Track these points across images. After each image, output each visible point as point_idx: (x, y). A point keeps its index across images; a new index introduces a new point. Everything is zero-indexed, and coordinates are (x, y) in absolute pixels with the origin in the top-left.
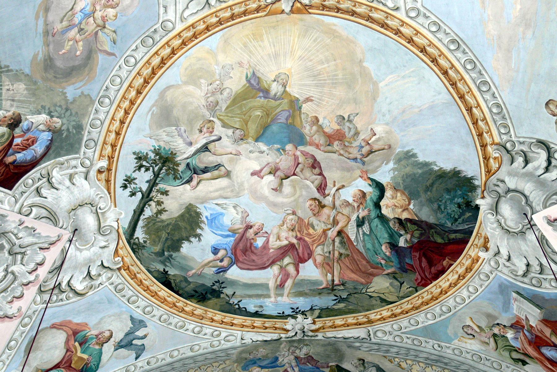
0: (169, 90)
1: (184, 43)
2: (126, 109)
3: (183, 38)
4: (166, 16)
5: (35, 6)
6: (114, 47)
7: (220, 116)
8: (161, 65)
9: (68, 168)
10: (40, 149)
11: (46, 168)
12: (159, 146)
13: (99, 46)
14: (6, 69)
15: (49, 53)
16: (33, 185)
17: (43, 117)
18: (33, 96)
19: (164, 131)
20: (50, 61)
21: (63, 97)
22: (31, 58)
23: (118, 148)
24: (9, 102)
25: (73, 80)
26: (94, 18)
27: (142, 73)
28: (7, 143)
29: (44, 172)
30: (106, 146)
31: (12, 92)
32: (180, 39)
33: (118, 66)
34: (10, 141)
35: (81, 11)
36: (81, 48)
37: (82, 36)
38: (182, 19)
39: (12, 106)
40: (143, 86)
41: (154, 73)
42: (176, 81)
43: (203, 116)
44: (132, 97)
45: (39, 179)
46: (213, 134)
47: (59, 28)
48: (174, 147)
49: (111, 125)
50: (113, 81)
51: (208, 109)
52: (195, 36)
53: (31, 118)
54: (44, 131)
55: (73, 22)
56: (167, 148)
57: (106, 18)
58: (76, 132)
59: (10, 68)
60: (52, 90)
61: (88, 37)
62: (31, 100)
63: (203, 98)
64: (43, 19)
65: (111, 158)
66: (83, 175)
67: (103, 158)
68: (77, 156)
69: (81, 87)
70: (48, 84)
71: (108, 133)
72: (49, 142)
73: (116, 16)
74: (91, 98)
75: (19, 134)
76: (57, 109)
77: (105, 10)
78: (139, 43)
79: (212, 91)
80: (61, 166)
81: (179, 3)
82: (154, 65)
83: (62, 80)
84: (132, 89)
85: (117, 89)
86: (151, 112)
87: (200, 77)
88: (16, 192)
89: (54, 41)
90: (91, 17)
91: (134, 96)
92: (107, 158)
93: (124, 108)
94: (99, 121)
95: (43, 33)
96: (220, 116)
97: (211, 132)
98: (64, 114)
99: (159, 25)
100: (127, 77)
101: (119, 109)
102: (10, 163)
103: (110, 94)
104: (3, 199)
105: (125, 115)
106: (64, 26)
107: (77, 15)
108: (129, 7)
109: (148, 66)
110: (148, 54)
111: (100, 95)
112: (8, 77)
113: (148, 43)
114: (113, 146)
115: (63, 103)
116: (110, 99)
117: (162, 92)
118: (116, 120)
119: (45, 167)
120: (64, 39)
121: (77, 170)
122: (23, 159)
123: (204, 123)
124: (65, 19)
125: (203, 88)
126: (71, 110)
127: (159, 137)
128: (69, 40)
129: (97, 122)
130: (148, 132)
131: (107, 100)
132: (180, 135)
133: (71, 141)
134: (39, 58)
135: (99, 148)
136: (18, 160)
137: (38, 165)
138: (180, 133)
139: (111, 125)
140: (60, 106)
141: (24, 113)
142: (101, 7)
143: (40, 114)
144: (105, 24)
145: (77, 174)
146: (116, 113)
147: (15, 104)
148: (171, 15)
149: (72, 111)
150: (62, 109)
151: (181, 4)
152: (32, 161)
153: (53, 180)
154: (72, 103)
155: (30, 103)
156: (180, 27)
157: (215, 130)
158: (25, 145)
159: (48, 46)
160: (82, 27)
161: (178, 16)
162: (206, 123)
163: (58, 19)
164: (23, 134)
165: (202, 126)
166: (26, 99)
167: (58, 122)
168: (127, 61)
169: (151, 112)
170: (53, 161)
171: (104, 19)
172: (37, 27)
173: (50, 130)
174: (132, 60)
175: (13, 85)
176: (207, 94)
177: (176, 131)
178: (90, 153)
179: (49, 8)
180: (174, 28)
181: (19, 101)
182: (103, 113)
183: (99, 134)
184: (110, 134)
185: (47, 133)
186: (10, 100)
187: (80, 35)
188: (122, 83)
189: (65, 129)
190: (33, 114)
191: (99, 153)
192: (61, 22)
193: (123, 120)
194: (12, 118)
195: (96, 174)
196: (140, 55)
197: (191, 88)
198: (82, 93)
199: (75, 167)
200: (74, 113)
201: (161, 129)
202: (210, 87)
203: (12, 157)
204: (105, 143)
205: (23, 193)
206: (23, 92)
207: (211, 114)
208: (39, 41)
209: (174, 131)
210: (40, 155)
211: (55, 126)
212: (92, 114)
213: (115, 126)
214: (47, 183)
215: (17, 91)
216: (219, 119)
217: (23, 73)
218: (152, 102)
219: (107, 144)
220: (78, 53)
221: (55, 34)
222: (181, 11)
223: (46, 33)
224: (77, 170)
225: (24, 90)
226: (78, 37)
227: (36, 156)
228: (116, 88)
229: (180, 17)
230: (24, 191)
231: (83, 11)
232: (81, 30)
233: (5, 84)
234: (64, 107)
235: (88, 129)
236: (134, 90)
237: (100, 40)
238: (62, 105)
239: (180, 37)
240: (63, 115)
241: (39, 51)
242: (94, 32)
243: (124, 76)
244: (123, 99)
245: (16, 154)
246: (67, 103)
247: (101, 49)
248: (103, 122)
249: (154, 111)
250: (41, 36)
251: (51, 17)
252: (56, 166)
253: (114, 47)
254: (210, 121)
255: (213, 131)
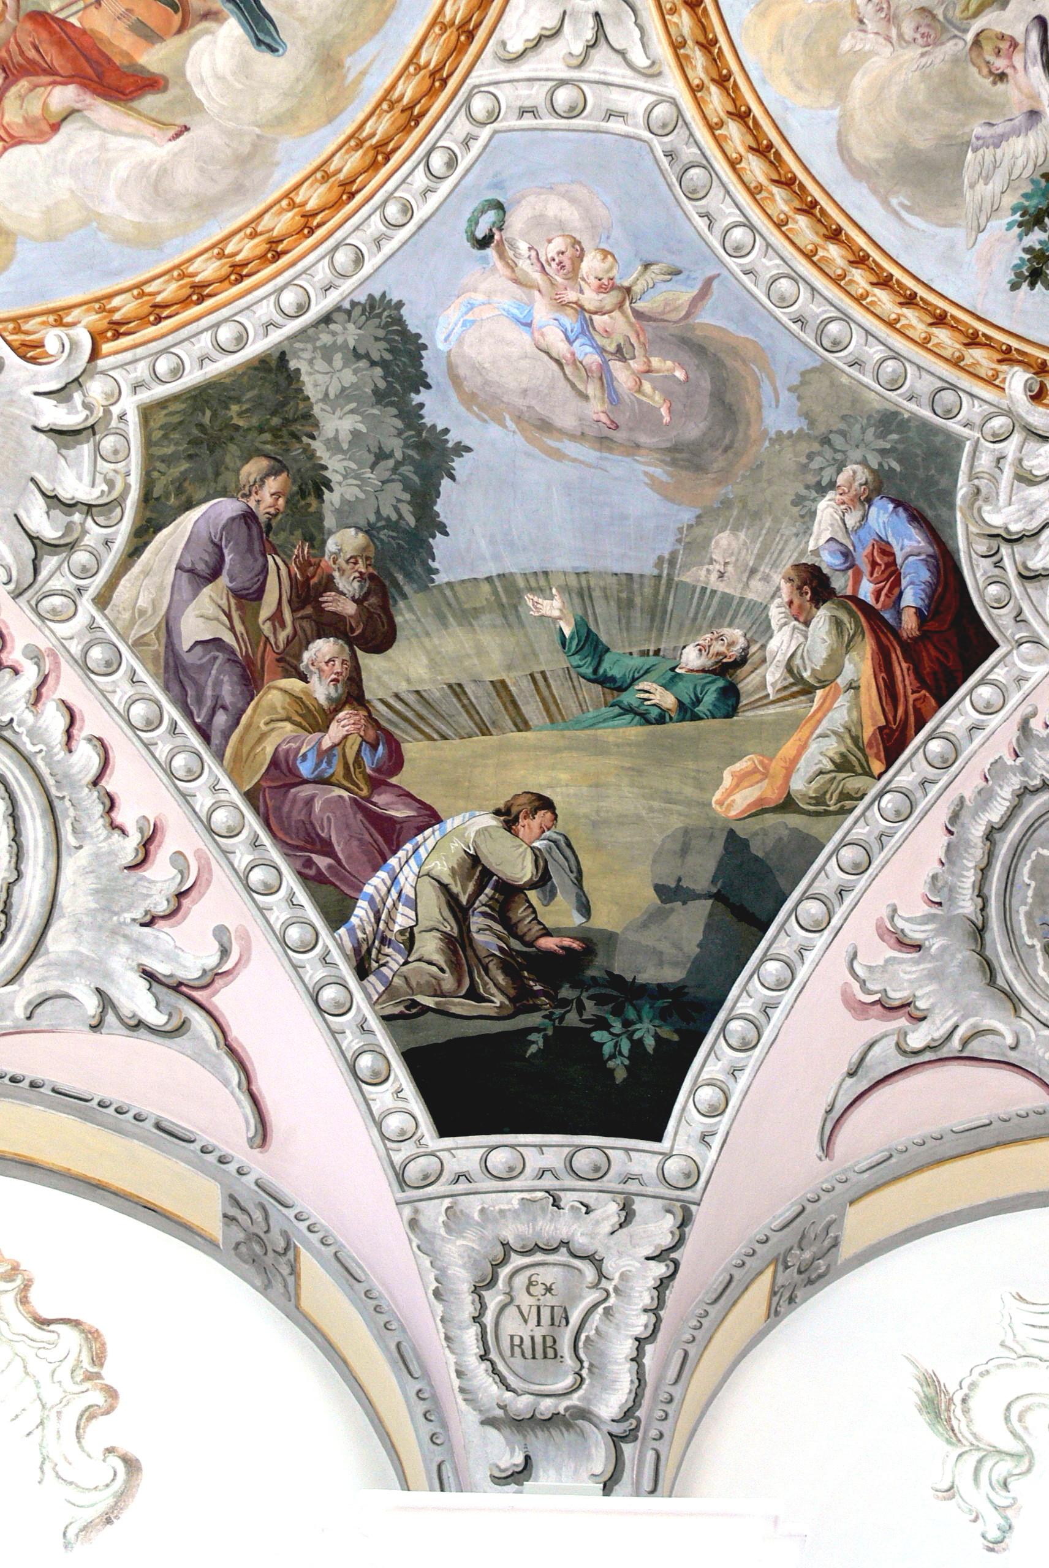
0: (849, 150)
1: (723, 80)
2: (875, 280)
3: (707, 81)
4: (634, 115)
5: (527, 454)
6: (688, 277)
7: (967, 8)
8: (772, 158)
9: (995, 480)
10: (910, 539)
11: (972, 537)
12: (1014, 210)
13: (674, 316)
14: (666, 566)
15: (658, 450)
16: (1008, 586)
17: (826, 508)
18: (761, 520)
19: (972, 186)
20: (681, 451)
21: (788, 442)
22: (655, 496)
23: (982, 328)
24: (756, 584)
25: (750, 405)
26: (596, 313)
27: (782, 216)
28: (862, 619)
29: (982, 547)
30: (968, 361)
31: (730, 568)
32: (708, 89)
33: (745, 279)
34: (861, 610)
35: (571, 343)
36: (669, 363)
37: (636, 353)
38: (653, 73)
39: (766, 579)
40: (819, 221)
41: (789, 183)
42: (828, 123)
43: (956, 60)
44: (843, 257)
45: (998, 565)
46: (1021, 41)
47: (599, 408)
48: (1031, 166)
49: (907, 332)
50: (782, 298)
51: (937, 43)
52: (708, 45)
53: (817, 540)
54: (865, 517)
55: (594, 367)
56: (1028, 188)
57: (605, 281)
58: (898, 433)
59: (667, 556)
60: (760, 466)
61: (642, 339)
62: (767, 525)
63: (900, 51)
64: (566, 441)
65: (1007, 357)
66: (1032, 445)
67: (1001, 376)
68: (968, 447)
69: (775, 390)
70: (741, 472)
71: (929, 346)
72: (900, 510)
73: (606, 253)
74: (814, 370)
75: (850, 583)
76: (817, 467)
77: (583, 279)
78: (695, 207)
79: (884, 23)
80: (981, 498)
81: (605, 73)
82: (767, 175)
83: (740, 436)
84: (821, 253)
85: (809, 295)
86: (903, 214)
87: (834, 50)
88: (1008, 634)
89: (631, 429)
90: (591, 320)
91: (843, 252)
92: (1004, 367)
93: (869, 288)
94: (885, 364)
95: (600, 450)
96: (967, 8)
97: (1014, 44)
98: (836, 451)
99: (655, 141)
100: (782, 259)
101: (869, 299)
102: (920, 626)
103: (818, 316)
104: (1015, 673)
105: (892, 288)
106: (598, 393)
107: (577, 355)
108: (587, 210)
109: (764, 194)
110: (731, 188)
111: (813, 343)
112: (686, 567)
113: (700, 183)
114: (973, 340)
115: (804, 447)
116: (832, 320)
117: (850, 170)
118: (899, 315)
119: (968, 539)
120: (632, 402)
121: (1010, 458)
122: (923, 590)
123: (979, 61)
124: (581, 387)
125: (867, 47)
126: (831, 431)
127: (987, 206)
128: (639, 391)
129: (889, 370)
130: (959, 234)
131: (834, 328)
132: (999, 141)
133: (919, 452)
134: (665, 478)
135: (965, 382)
136: (920, 604)
137: (956, 557)
138: (991, 141)
139: (910, 333)
140: (811, 456)
141: (796, 554)
142: (573, 289)
143: (813, 514)
144: (620, 288)
145: (1020, 460)
146: (878, 311)
147: (764, 569)
148: (636, 103)
149: (834, 428)
150: (819, 454)
151: (608, 69)
152: (938, 572)
153: (1014, 528)
154: (812, 423)
155: (774, 531)
156: (673, 85)
157: (1008, 32)
158: (885, 575)
159: (638, 446)
160: (612, 348)
161: (641, 83)
162: (980, 55)
163: (575, 403)
164: (854, 574)
165: (985, 71)
166: (761, 539)
167: (854, 472)
168: (737, 248)
169: (903, 214)
170: (959, 516)
171: (605, 287)
172: (582, 462)
173: (869, 501)
174: (738, 234)
175: (712, 561)
176: (888, 39)
177: (981, 152)
178: (971, 410)
179: (542, 420)
180: (674, 103)
181: (760, 557)
182: (866, 348)
183: (924, 373)
184: (934, 341)
185: (873, 510)
186: (749, 578)
187: (634, 358)
188: (796, 278)
189: (880, 459)
190: (807, 531)
191: (981, 384)
192: (586, 397)
193: (904, 296)
194: (800, 588)
195: (1041, 409)
196: (728, 211)
197: (860, 84)
198: (791, 389)
199: (999, 459)
200: (842, 426)
201: (962, 196)
202: (870, 26)
203: (905, 617)
204: (956, 363)
205: (1019, 618)
206: (741, 541)
207: (955, 36)
208: (619, 466)
209: (979, 158)
210: (930, 543)
211: (861, 485)
212: (860, 377)
213: (914, 322)
214: (1018, 548)
215: (732, 554)
216: (977, 14)
217: (690, 527)
218: (874, 204)
219: (962, 358)
220: (680, 374)
221: (613, 422)
222: (629, 73)
223: (603, 442)
224: (1010, 458)
225: (737, 538)
226: (636, 365)
227: (929, 556)
228: (805, 293)
229: (644, 79)
230: (1014, 614)
231: (572, 336)
232: (620, 353)
233: (703, 578)
234: (816, 447)
235: (900, 400)
236: (824, 249)
237: (660, 310)
238: (807, 451)
239: (701, 87)
240: (839, 456)
241: (646, 473)
242: (633, 320)
243: (778, 266)
244: (842, 283)
245: (903, 604)
246: (808, 434)
247: (683, 313)
248: (892, 354)
249: (902, 205)
250: (606, 459)
251: (566, 420)
252: (975, 511)
253: (688, 277)
254: (977, 42)
255: (1012, 39)
